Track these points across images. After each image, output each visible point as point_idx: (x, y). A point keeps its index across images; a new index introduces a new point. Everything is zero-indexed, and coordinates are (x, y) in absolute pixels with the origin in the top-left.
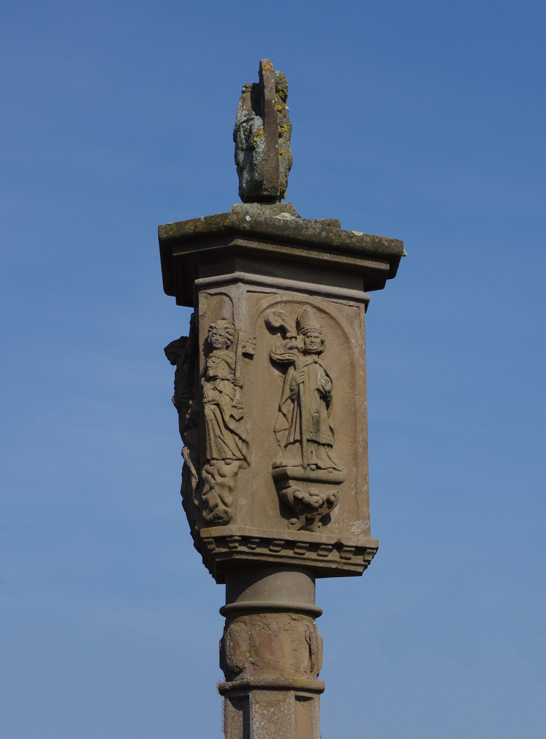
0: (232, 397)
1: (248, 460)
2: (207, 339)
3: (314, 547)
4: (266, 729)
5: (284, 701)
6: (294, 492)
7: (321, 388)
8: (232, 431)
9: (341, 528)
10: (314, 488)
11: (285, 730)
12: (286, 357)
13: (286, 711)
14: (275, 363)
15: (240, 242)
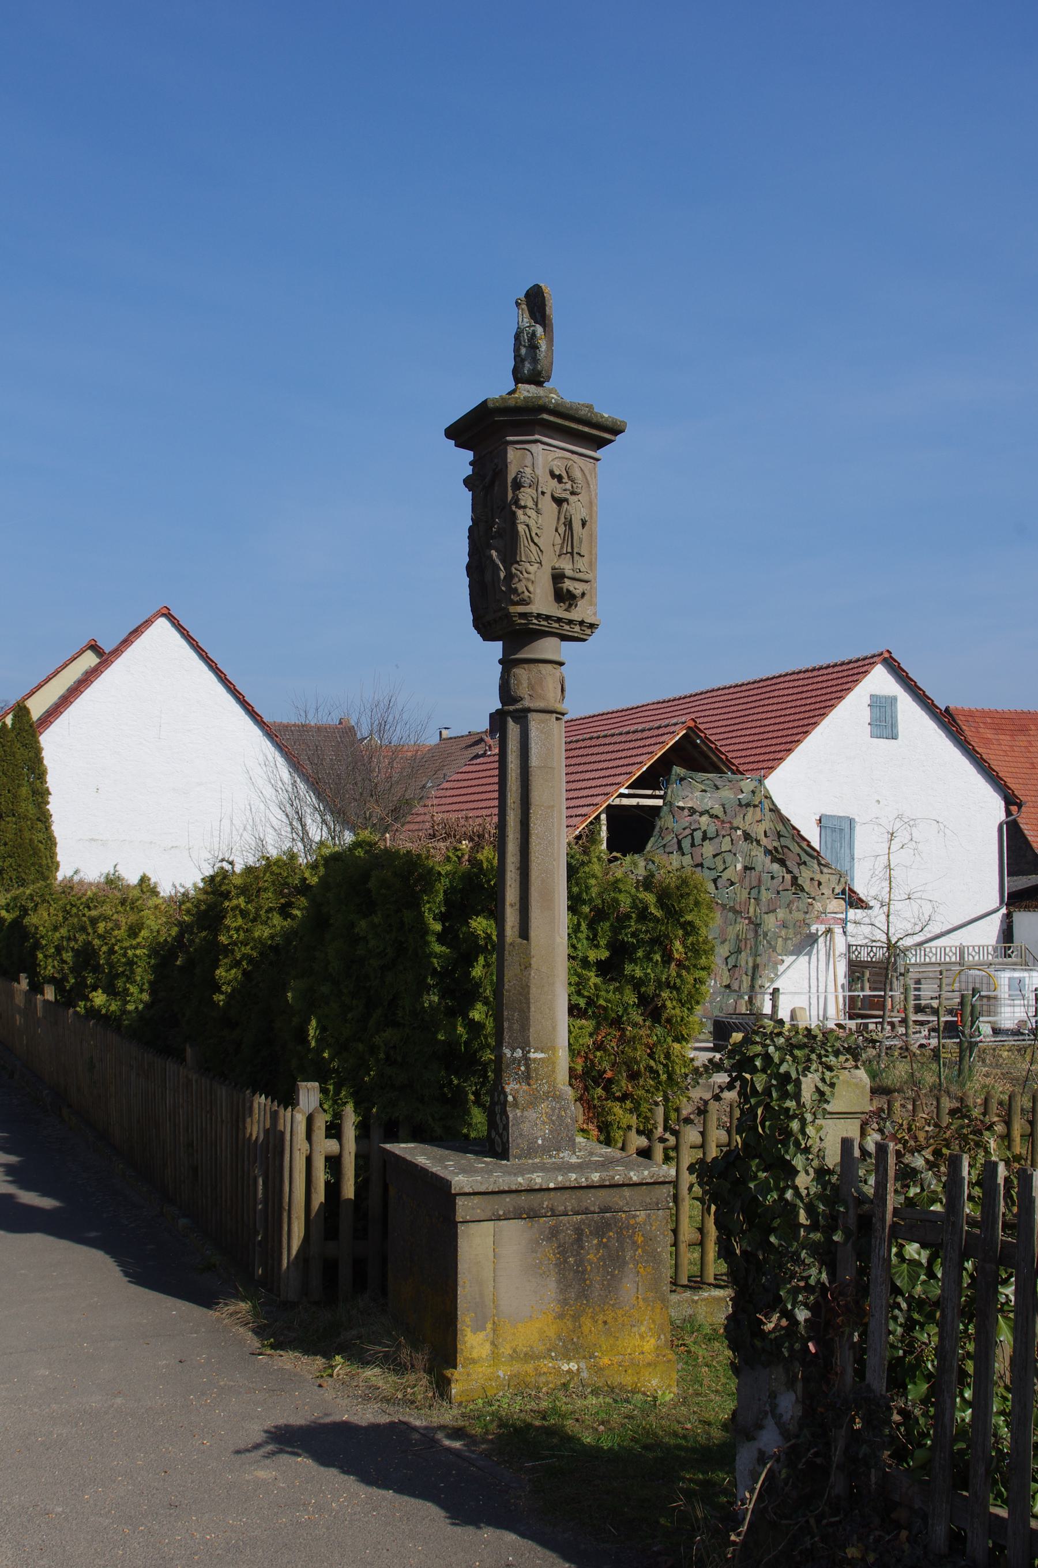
2: (515, 479)
3: (570, 622)
8: (535, 544)
9: (580, 612)
10: (577, 584)
14: (554, 499)
15: (545, 416)
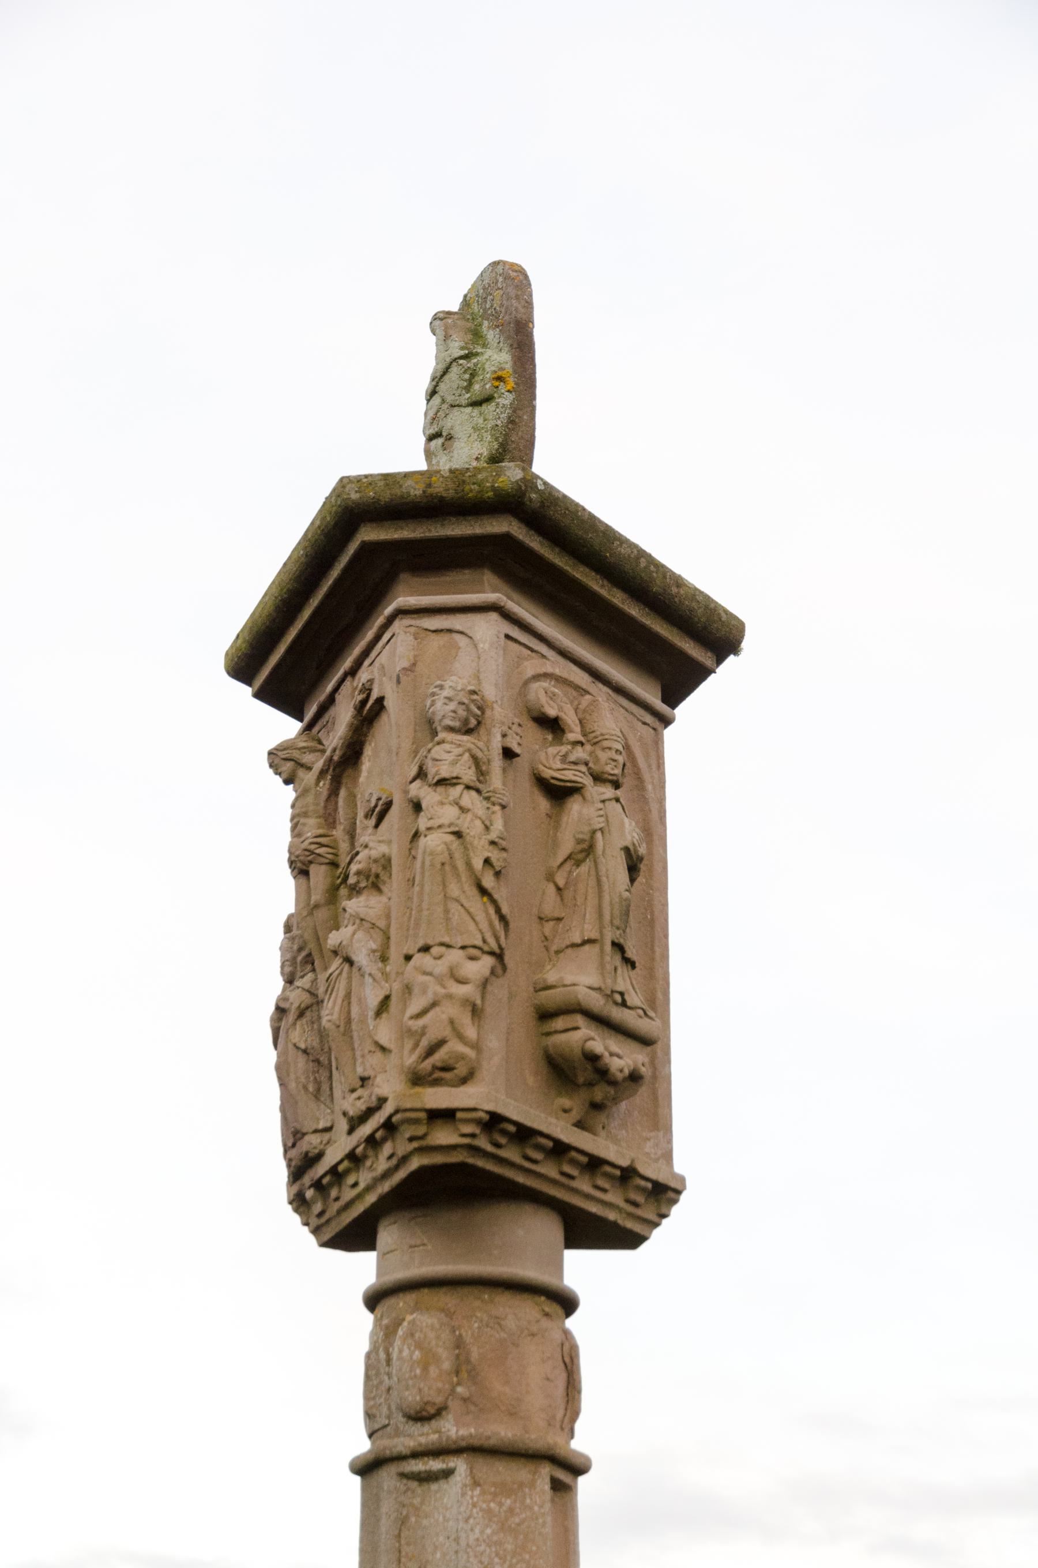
0: (488, 823)
1: (507, 959)
4: (495, 1543)
5: (532, 1485)
6: (586, 1041)
7: (632, 848)
11: (534, 1548)
12: (569, 775)
13: (536, 1508)
